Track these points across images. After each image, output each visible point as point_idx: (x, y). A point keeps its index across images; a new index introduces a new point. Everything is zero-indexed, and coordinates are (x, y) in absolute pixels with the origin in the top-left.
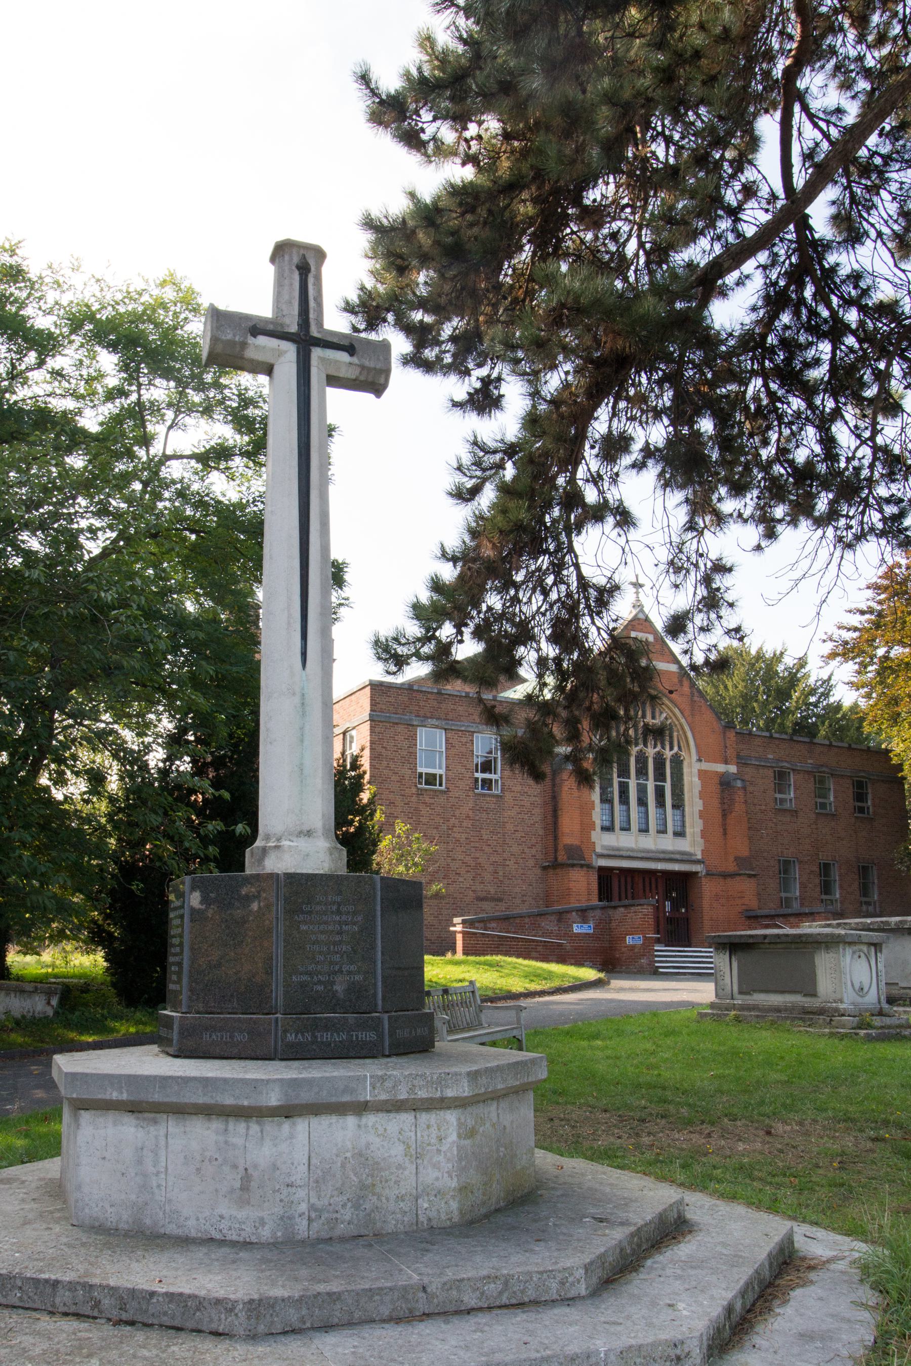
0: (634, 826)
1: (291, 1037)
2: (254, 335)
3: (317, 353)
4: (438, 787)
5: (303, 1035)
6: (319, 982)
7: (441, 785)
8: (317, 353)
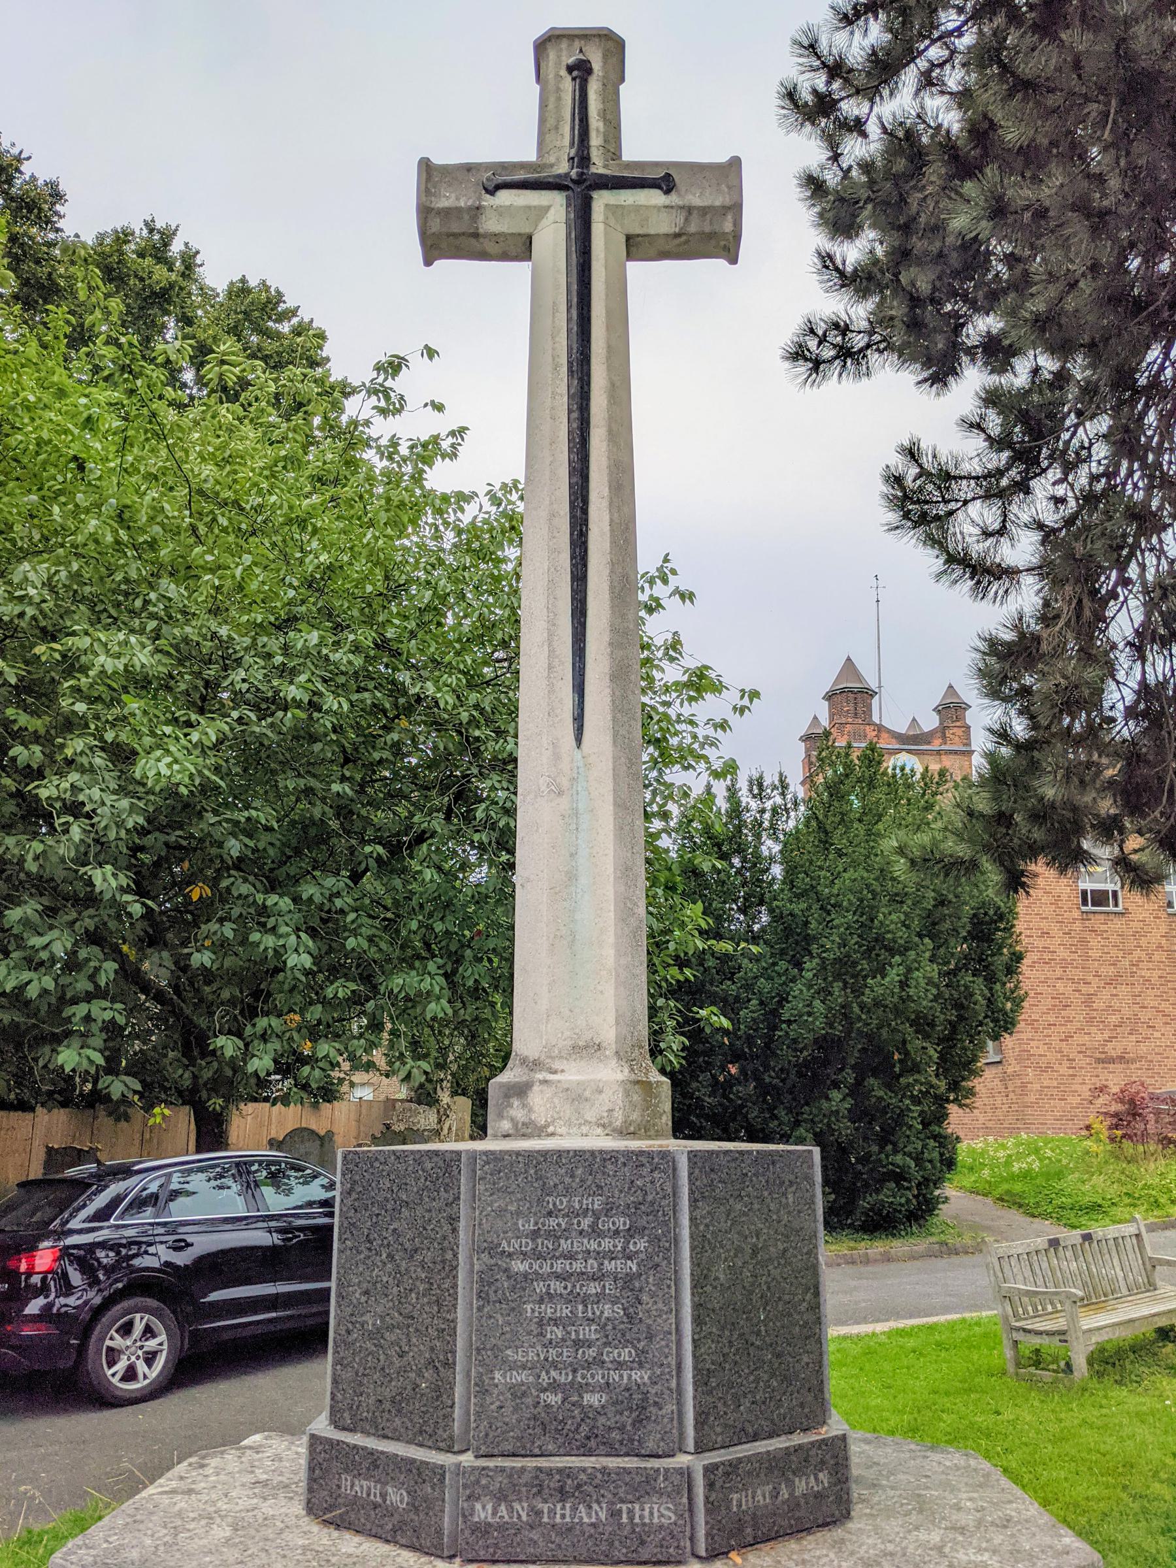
0: (1112, 1242)
1: (483, 1512)
2: (492, 191)
3: (602, 200)
4: (1111, 908)
5: (511, 1509)
6: (554, 1387)
7: (1116, 905)
8: (602, 200)
